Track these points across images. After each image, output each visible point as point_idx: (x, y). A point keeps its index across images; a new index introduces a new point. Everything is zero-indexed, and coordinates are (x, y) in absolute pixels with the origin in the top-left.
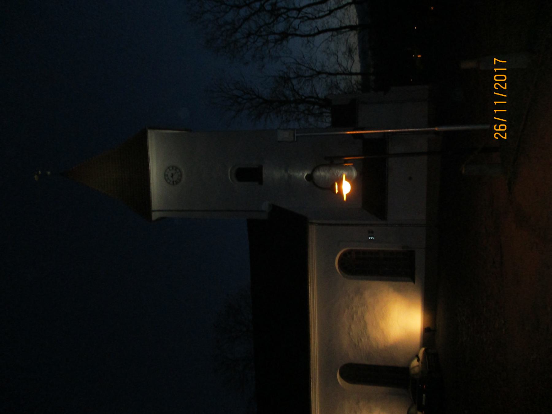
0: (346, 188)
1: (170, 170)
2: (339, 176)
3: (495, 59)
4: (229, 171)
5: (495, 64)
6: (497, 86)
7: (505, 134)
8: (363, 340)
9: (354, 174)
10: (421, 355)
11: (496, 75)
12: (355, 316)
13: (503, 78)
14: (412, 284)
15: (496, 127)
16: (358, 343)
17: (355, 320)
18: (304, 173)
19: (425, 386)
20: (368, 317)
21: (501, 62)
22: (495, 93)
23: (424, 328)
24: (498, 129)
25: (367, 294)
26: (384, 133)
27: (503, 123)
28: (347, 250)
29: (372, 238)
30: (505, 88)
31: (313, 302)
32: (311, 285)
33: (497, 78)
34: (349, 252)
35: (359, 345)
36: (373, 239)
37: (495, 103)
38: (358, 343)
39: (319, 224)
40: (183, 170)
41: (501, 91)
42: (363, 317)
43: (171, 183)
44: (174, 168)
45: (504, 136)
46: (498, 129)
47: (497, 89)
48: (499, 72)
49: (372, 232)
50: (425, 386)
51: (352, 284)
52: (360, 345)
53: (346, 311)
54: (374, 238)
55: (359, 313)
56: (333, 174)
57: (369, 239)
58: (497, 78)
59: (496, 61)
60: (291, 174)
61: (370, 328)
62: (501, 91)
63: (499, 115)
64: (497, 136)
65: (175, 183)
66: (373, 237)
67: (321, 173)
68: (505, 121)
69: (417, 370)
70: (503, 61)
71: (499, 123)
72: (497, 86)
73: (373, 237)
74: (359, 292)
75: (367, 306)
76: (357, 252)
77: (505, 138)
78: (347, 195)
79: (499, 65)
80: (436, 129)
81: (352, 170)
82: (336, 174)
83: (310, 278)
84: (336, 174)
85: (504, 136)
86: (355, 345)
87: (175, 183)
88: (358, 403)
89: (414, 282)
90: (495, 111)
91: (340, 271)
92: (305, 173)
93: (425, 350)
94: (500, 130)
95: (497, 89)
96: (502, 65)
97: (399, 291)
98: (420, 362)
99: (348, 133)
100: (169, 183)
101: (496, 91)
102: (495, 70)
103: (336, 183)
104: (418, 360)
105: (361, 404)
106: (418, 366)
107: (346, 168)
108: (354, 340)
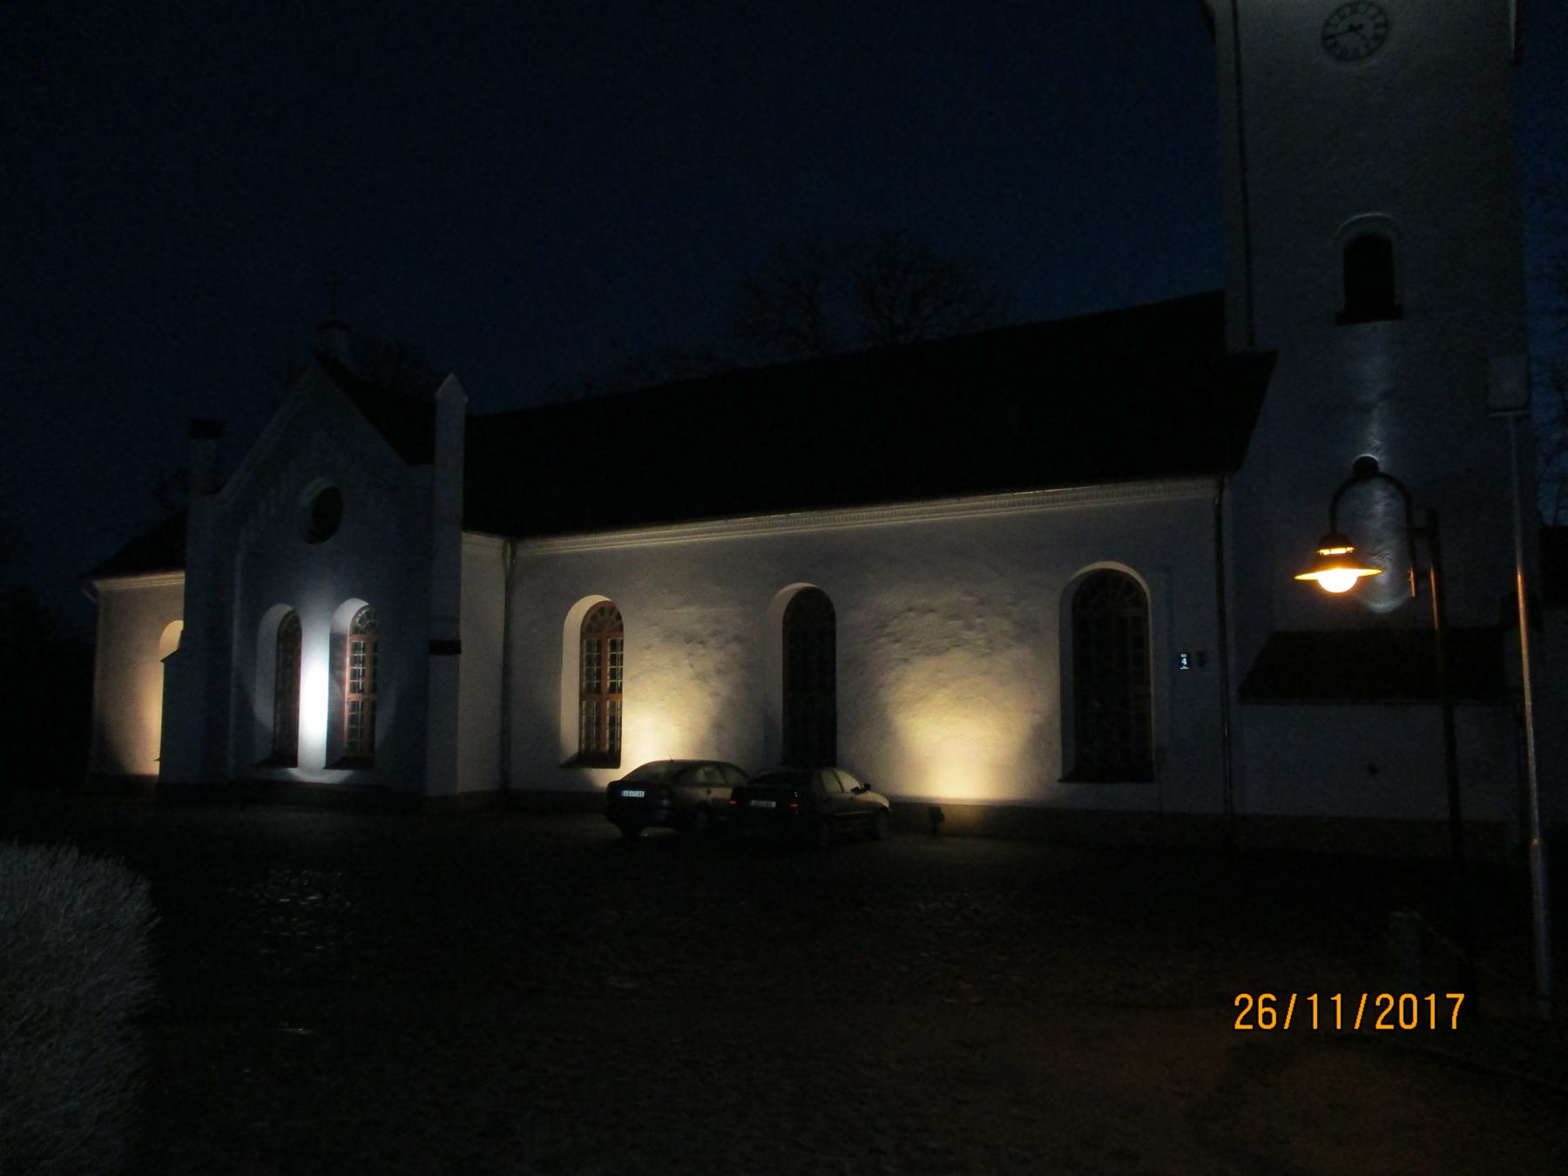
0: (1337, 580)
1: (1377, 26)
2: (1375, 559)
3: (1461, 997)
4: (1377, 214)
5: (1449, 996)
6: (1385, 1002)
7: (1436, 1026)
8: (897, 646)
9: (1382, 605)
10: (870, 796)
11: (1417, 999)
12: (961, 622)
13: (1408, 1020)
14: (1058, 774)
15: (1269, 999)
16: (889, 635)
17: (951, 623)
18: (1381, 452)
19: (795, 805)
20: (958, 659)
21: (1452, 1015)
22: (1365, 996)
23: (938, 804)
24: (1264, 1007)
25: (1020, 653)
26: (1522, 691)
27: (1281, 1020)
28: (1145, 594)
29: (1185, 661)
30: (1379, 1026)
31: (977, 508)
32: (1036, 498)
33: (1408, 1002)
34: (1140, 601)
35: (884, 636)
36: (1183, 665)
37: (1338, 998)
38: (889, 635)
39: (1219, 506)
40: (1373, 62)
41: (1372, 1012)
42: (958, 646)
43: (1330, 30)
44: (1381, 31)
45: (1383, 1023)
46: (1264, 1007)
47: (1378, 1003)
48: (1424, 1007)
49: (1202, 663)
50: (795, 805)
51: (1048, 612)
52: (882, 640)
53: (970, 599)
54: (1184, 668)
55: (968, 635)
56: (1379, 542)
57: (1182, 656)
58: (1408, 1002)
59: (1457, 1000)
60: (1375, 412)
61: (931, 663)
62: (1372, 1012)
63: (1304, 1008)
64: (1244, 1002)
65: (1329, 41)
66: (1187, 666)
67: (1383, 504)
68: (1286, 1026)
69: (832, 787)
70: (1457, 1018)
71: (1281, 1008)
72: (1385, 1002)
73: (1187, 666)
74: (1025, 631)
75: (987, 654)
76: (1140, 622)
77: (1238, 1026)
78: (1312, 585)
79: (1445, 1007)
80: (1536, 841)
81: (1394, 597)
82: (1379, 551)
83: (1058, 493)
84: (1380, 547)
85: (1383, 1023)
86: (883, 626)
87: (1331, 41)
88: (737, 638)
89: (1060, 781)
90: (1314, 998)
91: (1081, 576)
92: (1382, 454)
93: (885, 807)
94: (1261, 1011)
95: (1378, 1003)
96: (1444, 1018)
97: (1037, 739)
98: (853, 795)
99: (1519, 578)
100: (1327, 24)
101: (1371, 1001)
102: (1432, 998)
103: (1350, 549)
104: (856, 791)
105: (735, 647)
106: (843, 790)
107: (1399, 581)
108: (896, 621)
